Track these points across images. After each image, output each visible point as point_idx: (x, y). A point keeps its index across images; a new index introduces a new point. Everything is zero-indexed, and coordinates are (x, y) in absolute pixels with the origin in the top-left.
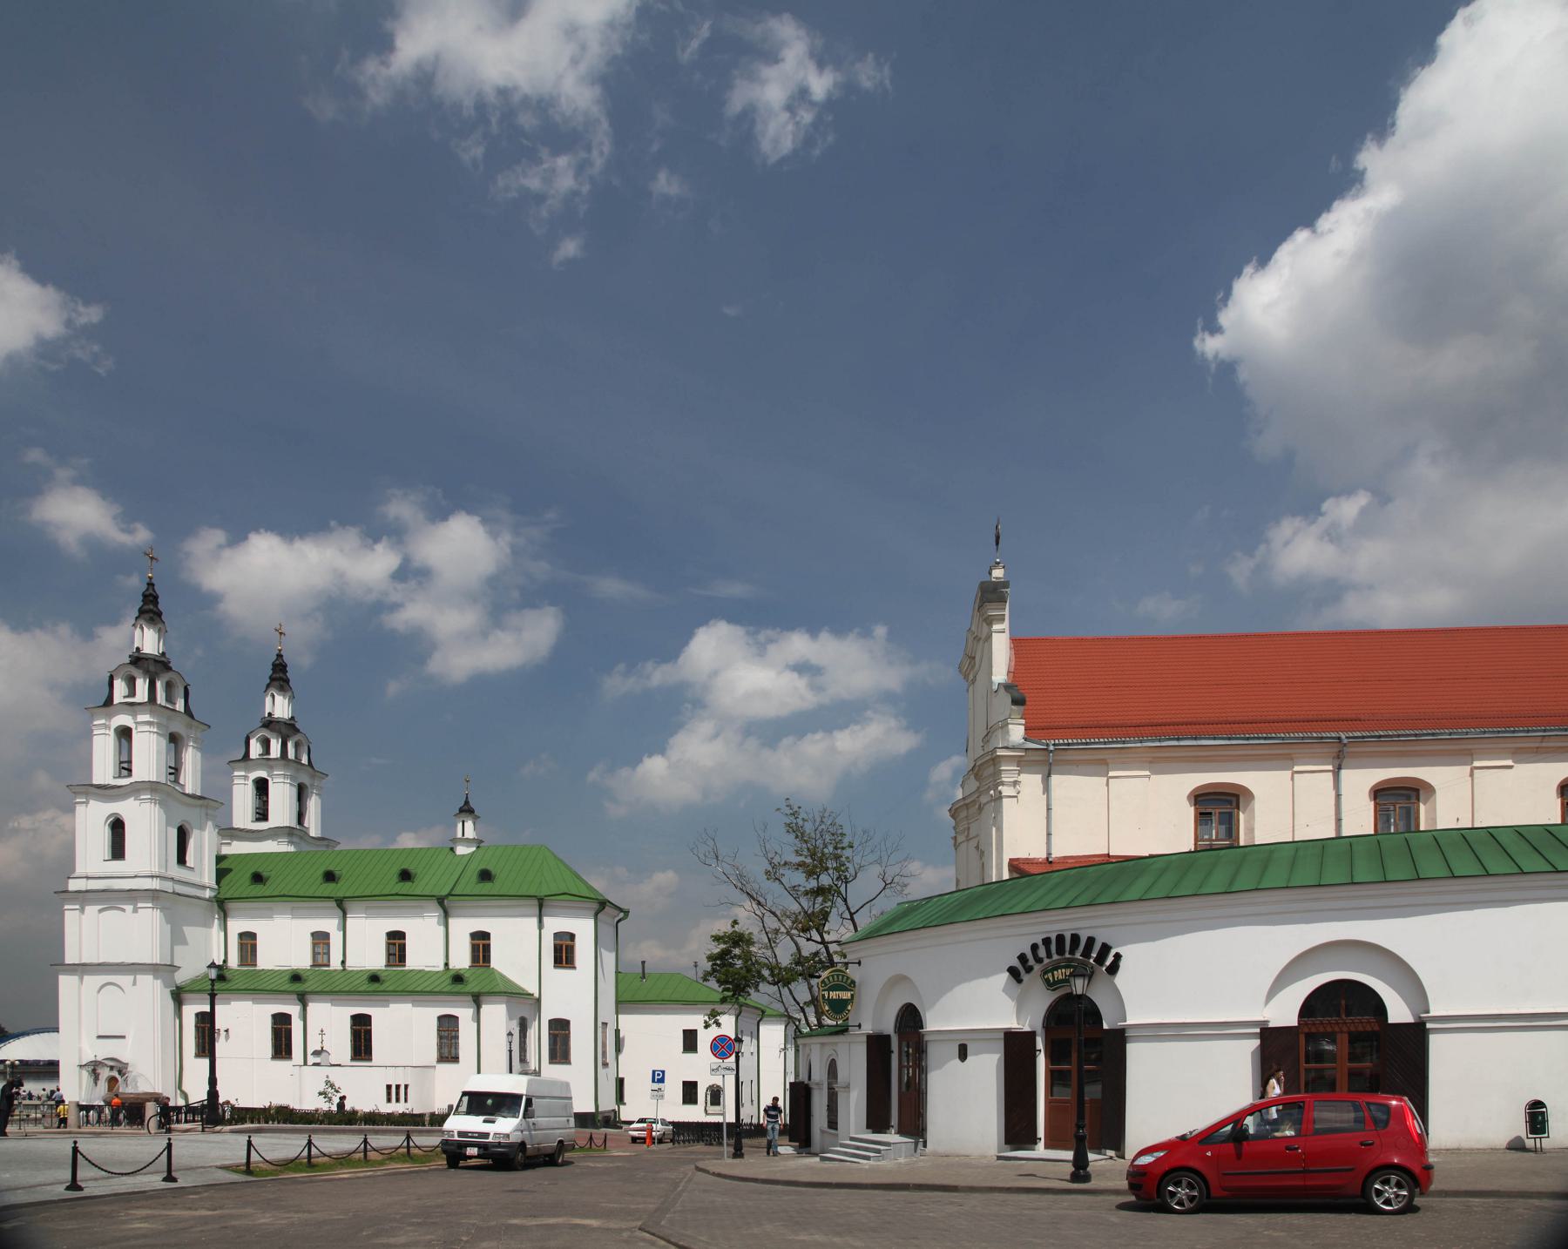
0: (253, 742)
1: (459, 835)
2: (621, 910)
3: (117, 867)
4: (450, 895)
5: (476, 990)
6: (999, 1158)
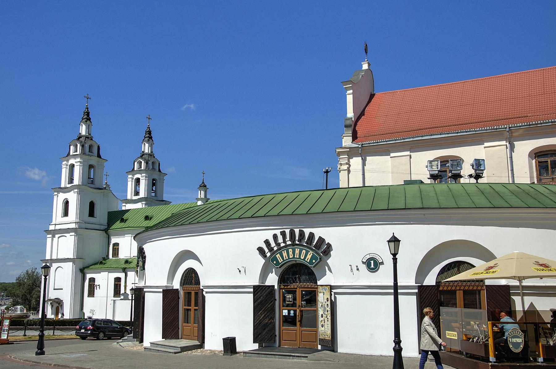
0: (136, 163)
1: (199, 197)
3: (66, 219)
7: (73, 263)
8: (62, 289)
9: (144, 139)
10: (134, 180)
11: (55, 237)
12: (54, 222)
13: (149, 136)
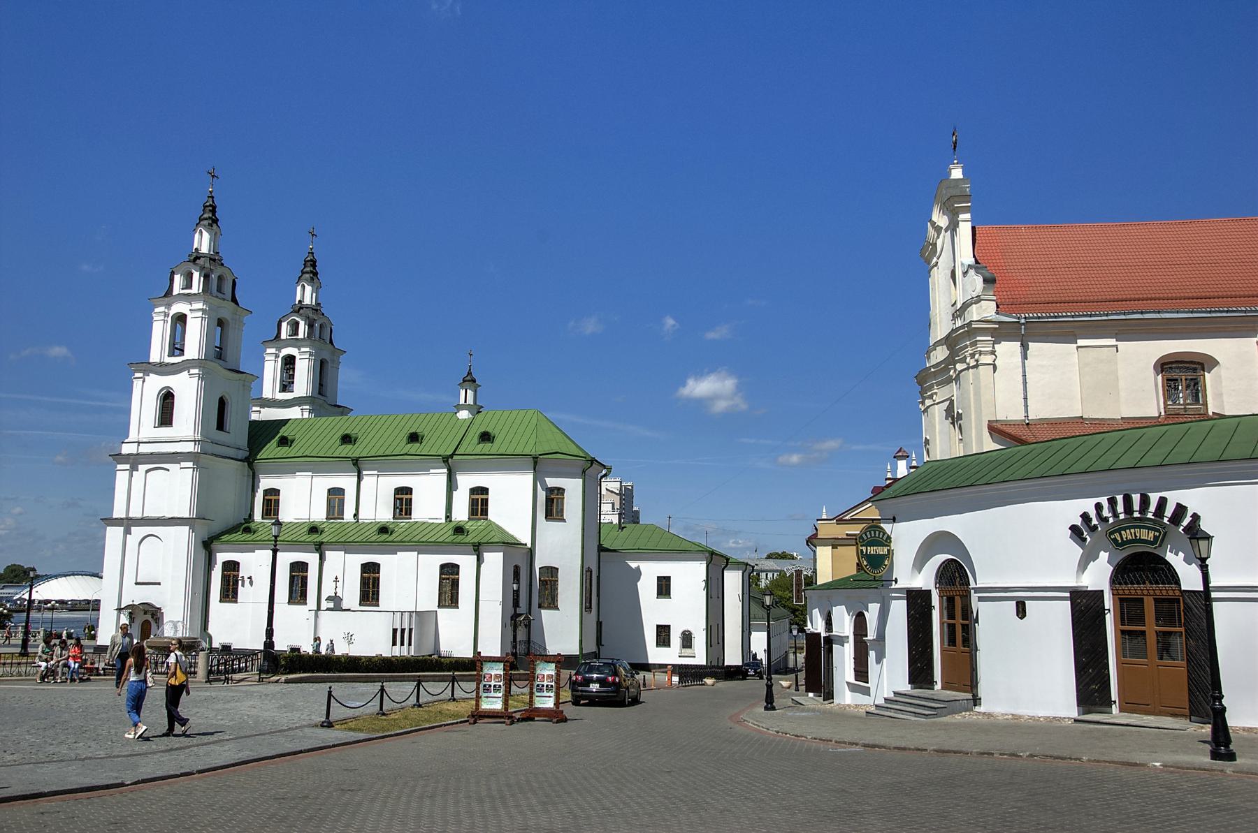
0: (284, 325)
1: (462, 401)
2: (604, 467)
3: (165, 432)
4: (454, 454)
5: (476, 540)
6: (1076, 721)
7: (190, 529)
8: (159, 584)
9: (301, 276)
10: (280, 360)
11: (138, 471)
12: (133, 436)
13: (311, 270)
